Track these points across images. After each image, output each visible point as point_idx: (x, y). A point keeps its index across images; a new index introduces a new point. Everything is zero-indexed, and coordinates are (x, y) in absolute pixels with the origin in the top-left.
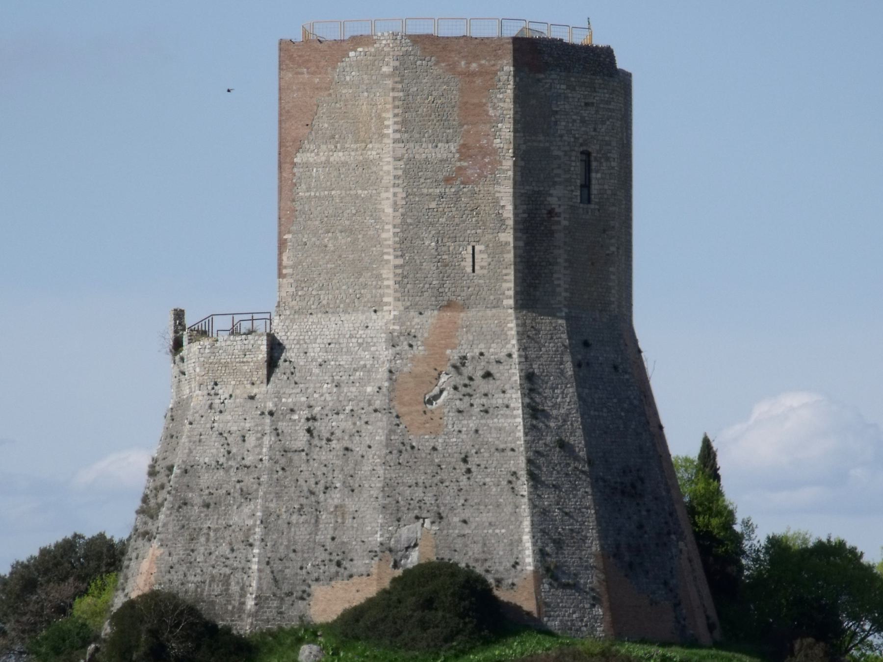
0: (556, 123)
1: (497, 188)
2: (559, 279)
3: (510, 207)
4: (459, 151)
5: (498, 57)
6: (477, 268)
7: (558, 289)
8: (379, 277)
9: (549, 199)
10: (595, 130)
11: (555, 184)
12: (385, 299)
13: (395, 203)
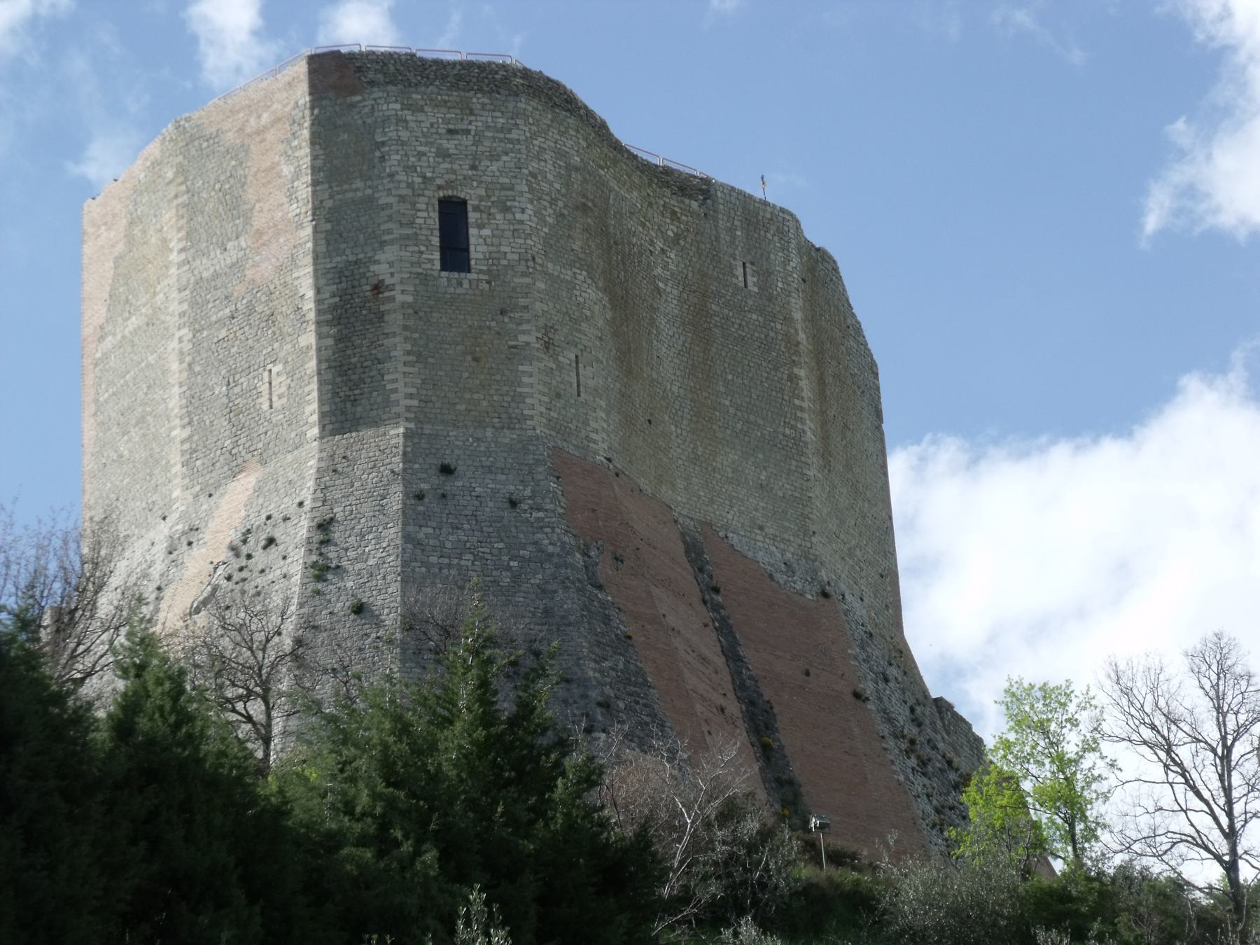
9: (373, 268)
10: (473, 167)
11: (383, 244)
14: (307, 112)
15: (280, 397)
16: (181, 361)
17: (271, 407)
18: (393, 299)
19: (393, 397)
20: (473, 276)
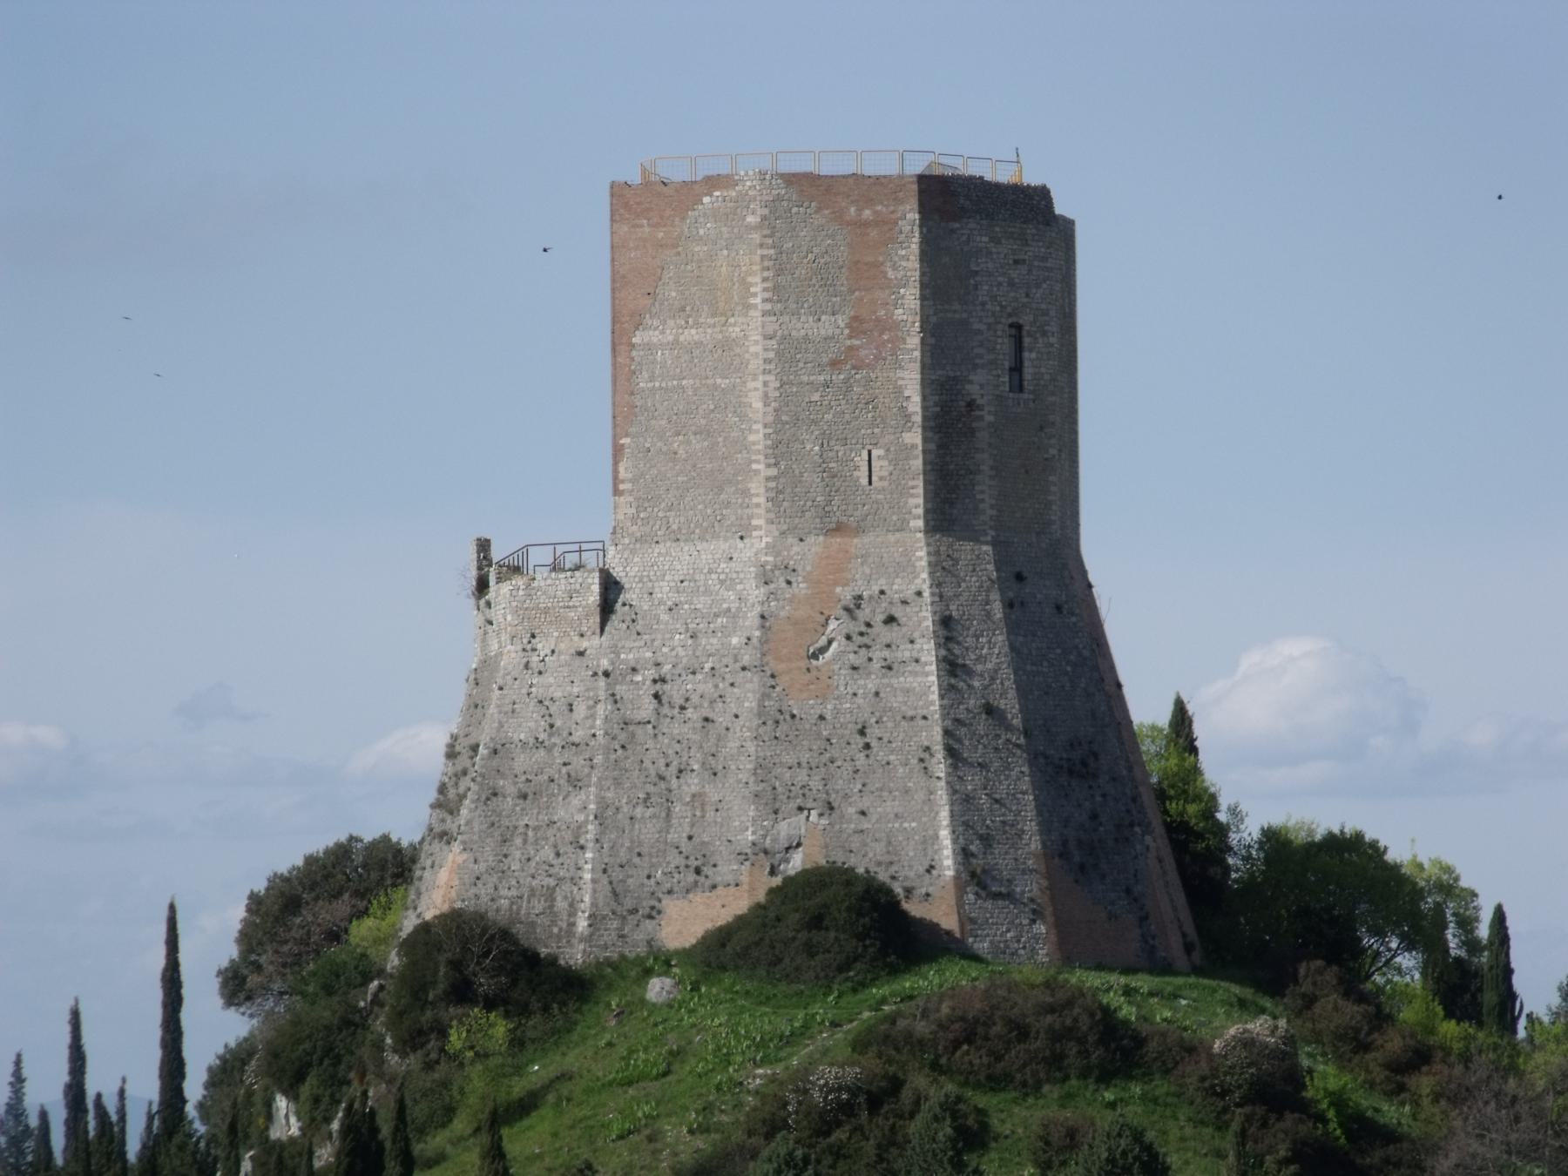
0: (976, 287)
1: (900, 374)
2: (982, 492)
3: (917, 399)
4: (848, 326)
5: (902, 202)
6: (874, 478)
7: (981, 506)
8: (745, 493)
9: (968, 387)
10: (1027, 295)
11: (975, 367)
12: (755, 522)
13: (766, 395)
14: (916, 229)
15: (881, 479)
16: (766, 405)
17: (870, 483)
18: (981, 418)
19: (981, 506)
20: (1026, 396)
